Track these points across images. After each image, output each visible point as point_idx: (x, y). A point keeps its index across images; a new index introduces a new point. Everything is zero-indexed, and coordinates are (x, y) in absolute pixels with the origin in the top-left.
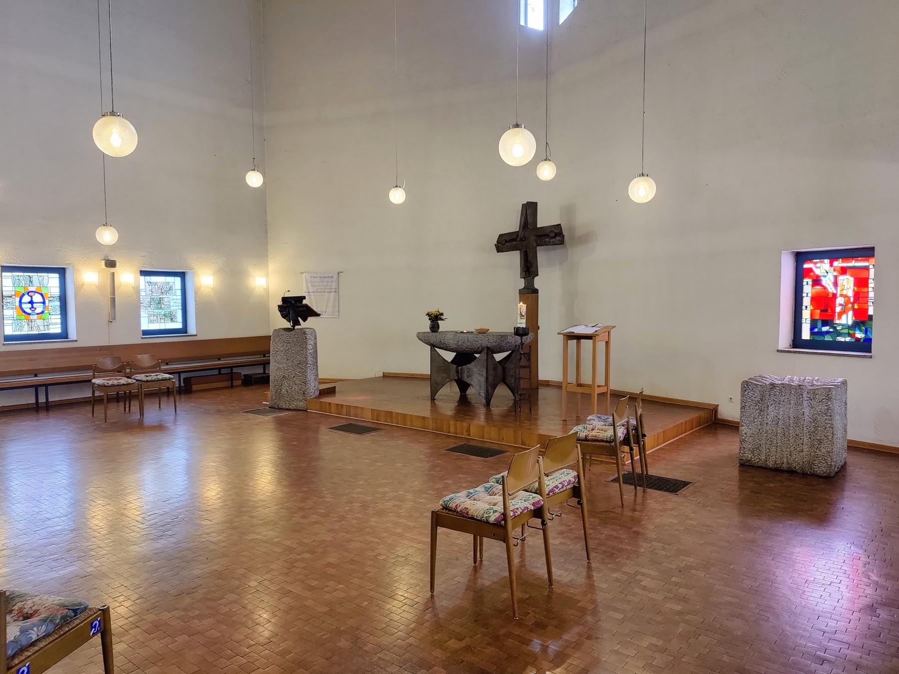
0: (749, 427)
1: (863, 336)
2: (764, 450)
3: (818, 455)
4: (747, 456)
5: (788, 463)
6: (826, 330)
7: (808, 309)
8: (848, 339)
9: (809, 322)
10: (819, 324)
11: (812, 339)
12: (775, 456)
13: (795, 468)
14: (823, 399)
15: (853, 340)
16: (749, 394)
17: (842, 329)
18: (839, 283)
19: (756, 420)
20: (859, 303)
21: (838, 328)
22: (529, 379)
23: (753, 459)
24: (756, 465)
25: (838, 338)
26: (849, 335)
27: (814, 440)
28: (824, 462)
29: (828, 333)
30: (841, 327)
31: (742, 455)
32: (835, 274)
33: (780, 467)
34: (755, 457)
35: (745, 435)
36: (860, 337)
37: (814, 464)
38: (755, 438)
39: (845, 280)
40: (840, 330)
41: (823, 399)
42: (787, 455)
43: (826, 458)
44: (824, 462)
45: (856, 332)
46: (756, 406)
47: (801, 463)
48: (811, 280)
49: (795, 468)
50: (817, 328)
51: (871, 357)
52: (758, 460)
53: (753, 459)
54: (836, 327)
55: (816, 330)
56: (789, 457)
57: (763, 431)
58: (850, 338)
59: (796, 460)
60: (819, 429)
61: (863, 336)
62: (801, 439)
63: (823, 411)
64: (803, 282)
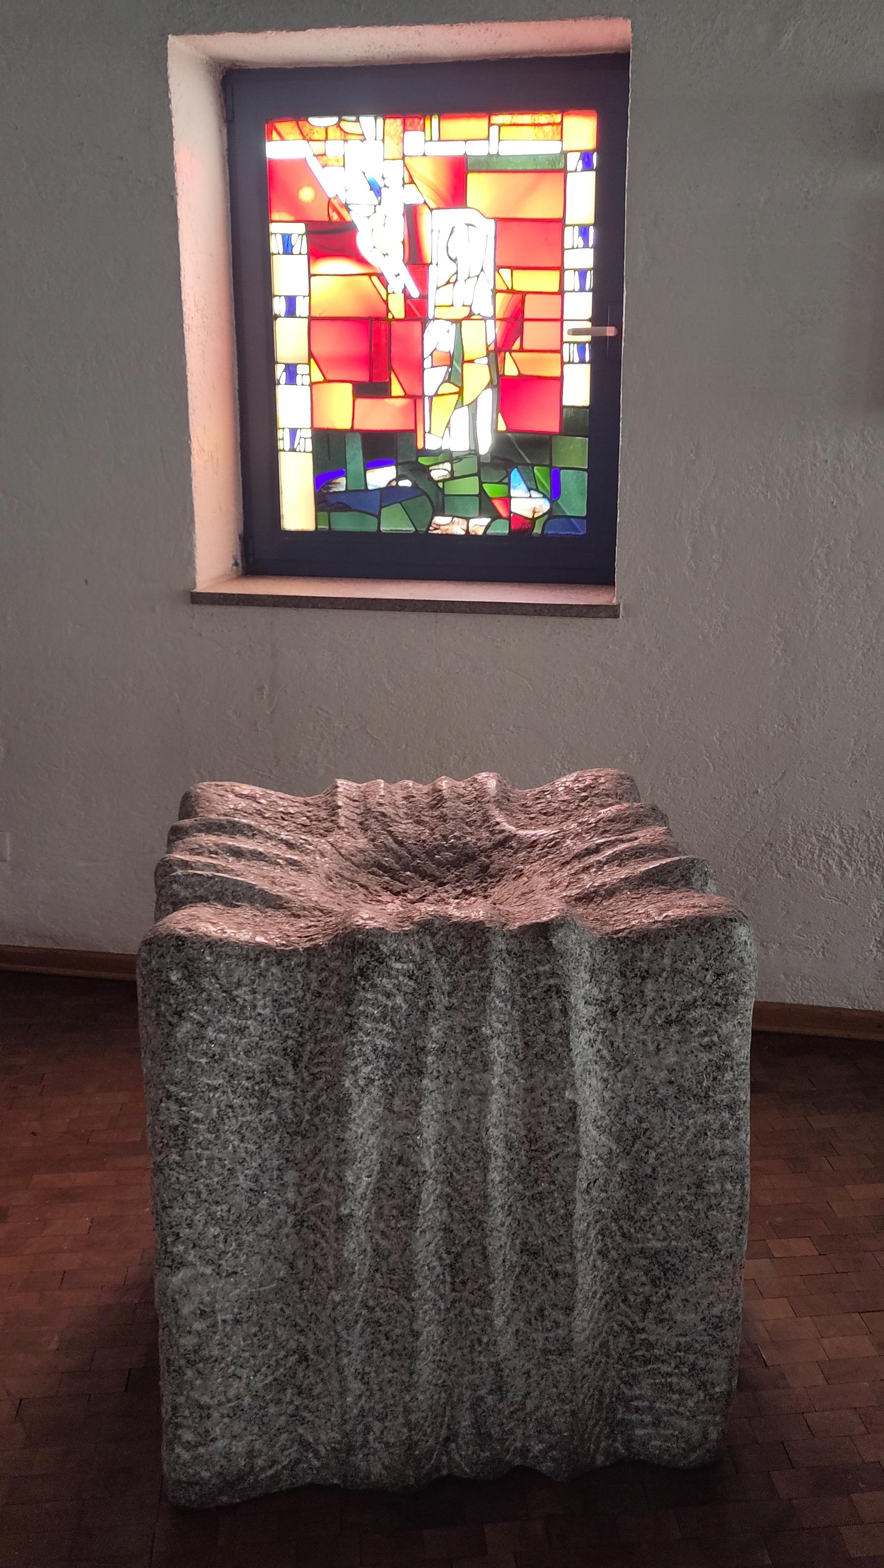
0: (226, 1265)
1: (544, 506)
2: (334, 1385)
3: (650, 1346)
4: (227, 1456)
5: (482, 1437)
6: (383, 484)
7: (299, 379)
8: (479, 525)
9: (309, 448)
10: (355, 455)
11: (324, 526)
12: (407, 1411)
13: (524, 1451)
14: (689, 1006)
15: (501, 528)
16: (210, 1033)
17: (453, 477)
18: (431, 247)
19: (264, 1203)
20: (522, 350)
21: (437, 474)
22: (558, 124)
23: (260, 1462)
24: (285, 1485)
25: (438, 520)
26: (485, 505)
27: (627, 1260)
28: (687, 1384)
29: (389, 494)
30: (448, 466)
31: (186, 1456)
32: (412, 196)
33: (437, 1469)
34: (271, 1443)
35: (198, 1326)
36: (529, 515)
37: (627, 1402)
38: (268, 1323)
39: (460, 230)
40: (444, 481)
41: (689, 1006)
42: (475, 1388)
43: (702, 1363)
44: (687, 1384)
45: (513, 493)
46: (260, 1109)
47: (559, 1422)
48: (301, 228)
49: (524, 1451)
50: (341, 473)
51: (612, 612)
52: (293, 1452)
53: (260, 1462)
54: (426, 470)
55: (341, 484)
56: (490, 1399)
57: (317, 1269)
58: (486, 521)
59: (530, 1405)
60: (661, 1190)
61: (544, 506)
62: (556, 1275)
63: (688, 1079)
64: (266, 236)
